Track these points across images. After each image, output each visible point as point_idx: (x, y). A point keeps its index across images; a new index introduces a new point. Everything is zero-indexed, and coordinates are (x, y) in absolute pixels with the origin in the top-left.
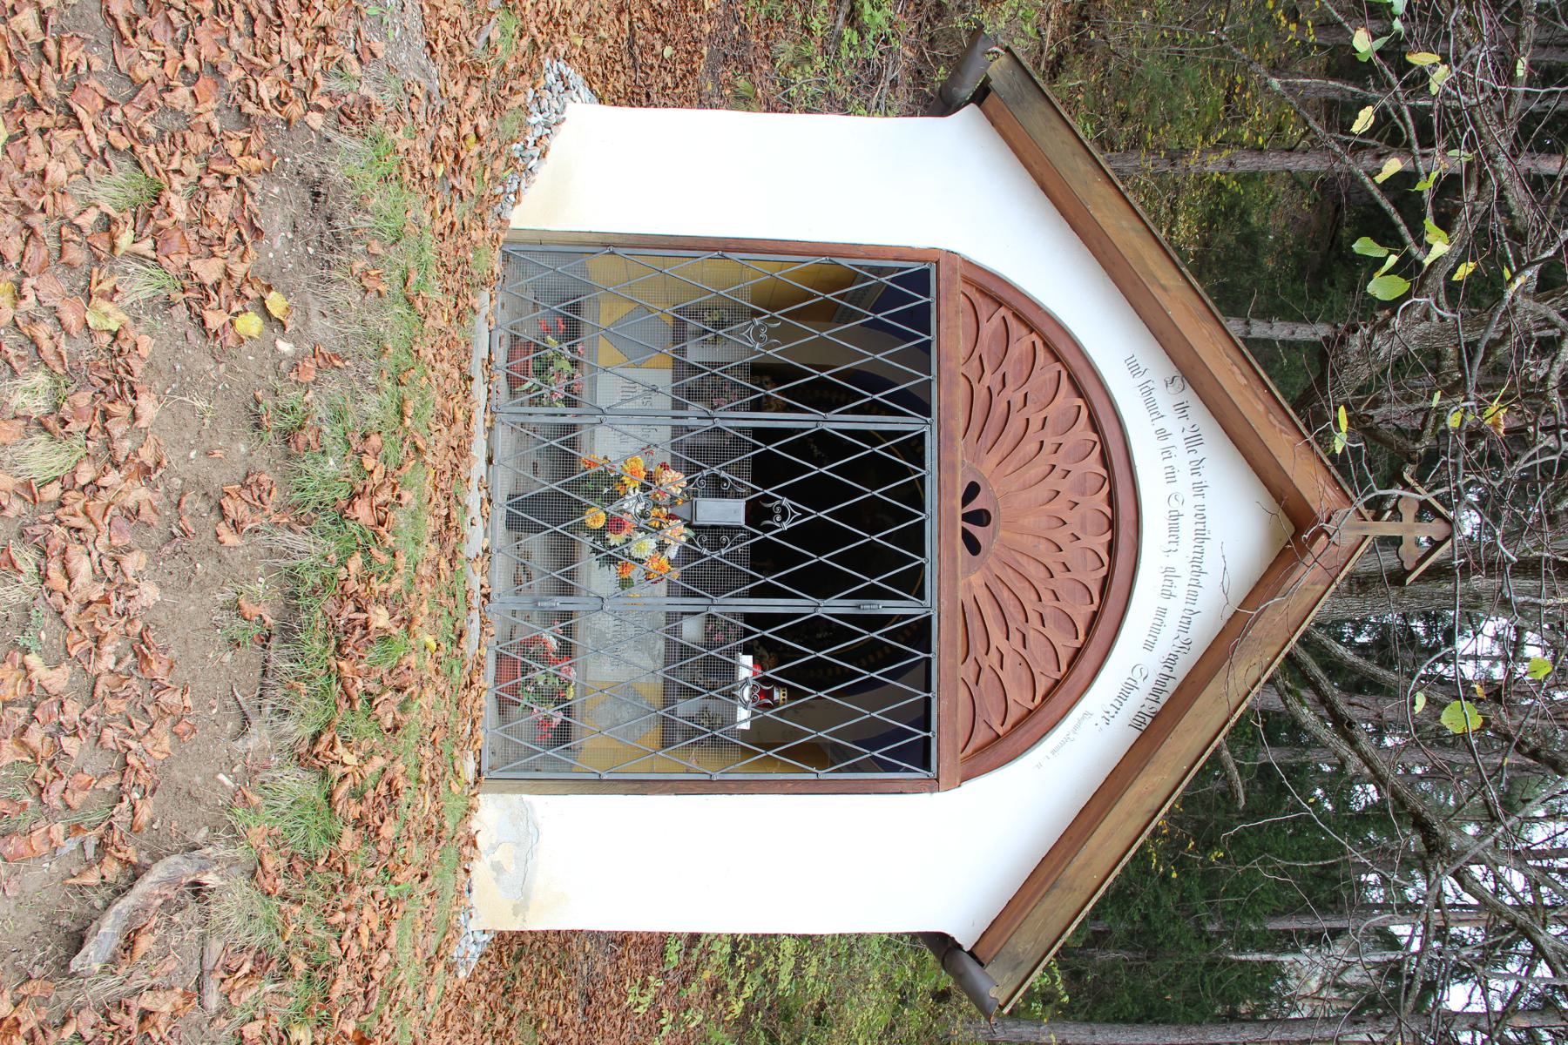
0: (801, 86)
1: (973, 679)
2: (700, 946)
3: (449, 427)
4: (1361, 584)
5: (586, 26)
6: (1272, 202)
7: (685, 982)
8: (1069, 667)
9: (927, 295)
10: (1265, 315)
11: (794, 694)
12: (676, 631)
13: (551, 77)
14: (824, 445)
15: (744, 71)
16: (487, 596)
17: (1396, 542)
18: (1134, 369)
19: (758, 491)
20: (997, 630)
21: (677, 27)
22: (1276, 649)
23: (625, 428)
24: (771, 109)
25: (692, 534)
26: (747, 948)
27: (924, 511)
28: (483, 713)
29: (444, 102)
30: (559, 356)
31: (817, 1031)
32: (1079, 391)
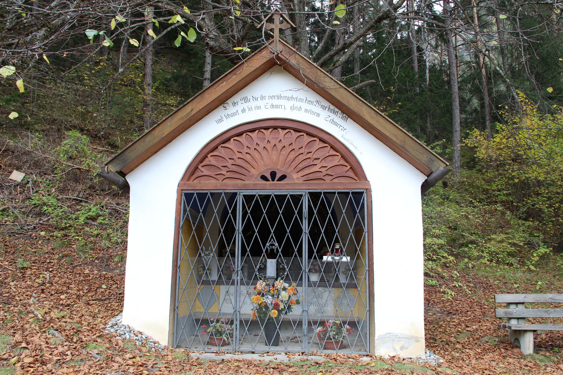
0: (118, 238)
1: (330, 177)
2: (429, 272)
3: (240, 368)
4: (296, 41)
5: (94, 317)
6: (163, 70)
7: (443, 278)
8: (326, 143)
9: (194, 194)
10: (202, 73)
11: (337, 241)
12: (315, 283)
13: (112, 330)
14: (247, 231)
15: (112, 259)
16: (303, 353)
17: (281, 31)
18: (220, 121)
19: (264, 254)
20: (314, 168)
21: (95, 283)
22: (319, 71)
23: (241, 303)
24: (126, 249)
25: (280, 278)
26: (430, 255)
27: (271, 195)
28: (346, 354)
29: (120, 371)
30: (215, 327)
31: (459, 229)
32: (228, 140)
